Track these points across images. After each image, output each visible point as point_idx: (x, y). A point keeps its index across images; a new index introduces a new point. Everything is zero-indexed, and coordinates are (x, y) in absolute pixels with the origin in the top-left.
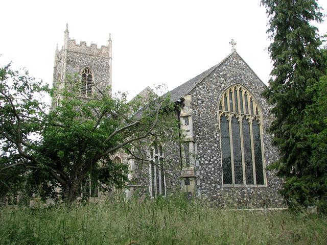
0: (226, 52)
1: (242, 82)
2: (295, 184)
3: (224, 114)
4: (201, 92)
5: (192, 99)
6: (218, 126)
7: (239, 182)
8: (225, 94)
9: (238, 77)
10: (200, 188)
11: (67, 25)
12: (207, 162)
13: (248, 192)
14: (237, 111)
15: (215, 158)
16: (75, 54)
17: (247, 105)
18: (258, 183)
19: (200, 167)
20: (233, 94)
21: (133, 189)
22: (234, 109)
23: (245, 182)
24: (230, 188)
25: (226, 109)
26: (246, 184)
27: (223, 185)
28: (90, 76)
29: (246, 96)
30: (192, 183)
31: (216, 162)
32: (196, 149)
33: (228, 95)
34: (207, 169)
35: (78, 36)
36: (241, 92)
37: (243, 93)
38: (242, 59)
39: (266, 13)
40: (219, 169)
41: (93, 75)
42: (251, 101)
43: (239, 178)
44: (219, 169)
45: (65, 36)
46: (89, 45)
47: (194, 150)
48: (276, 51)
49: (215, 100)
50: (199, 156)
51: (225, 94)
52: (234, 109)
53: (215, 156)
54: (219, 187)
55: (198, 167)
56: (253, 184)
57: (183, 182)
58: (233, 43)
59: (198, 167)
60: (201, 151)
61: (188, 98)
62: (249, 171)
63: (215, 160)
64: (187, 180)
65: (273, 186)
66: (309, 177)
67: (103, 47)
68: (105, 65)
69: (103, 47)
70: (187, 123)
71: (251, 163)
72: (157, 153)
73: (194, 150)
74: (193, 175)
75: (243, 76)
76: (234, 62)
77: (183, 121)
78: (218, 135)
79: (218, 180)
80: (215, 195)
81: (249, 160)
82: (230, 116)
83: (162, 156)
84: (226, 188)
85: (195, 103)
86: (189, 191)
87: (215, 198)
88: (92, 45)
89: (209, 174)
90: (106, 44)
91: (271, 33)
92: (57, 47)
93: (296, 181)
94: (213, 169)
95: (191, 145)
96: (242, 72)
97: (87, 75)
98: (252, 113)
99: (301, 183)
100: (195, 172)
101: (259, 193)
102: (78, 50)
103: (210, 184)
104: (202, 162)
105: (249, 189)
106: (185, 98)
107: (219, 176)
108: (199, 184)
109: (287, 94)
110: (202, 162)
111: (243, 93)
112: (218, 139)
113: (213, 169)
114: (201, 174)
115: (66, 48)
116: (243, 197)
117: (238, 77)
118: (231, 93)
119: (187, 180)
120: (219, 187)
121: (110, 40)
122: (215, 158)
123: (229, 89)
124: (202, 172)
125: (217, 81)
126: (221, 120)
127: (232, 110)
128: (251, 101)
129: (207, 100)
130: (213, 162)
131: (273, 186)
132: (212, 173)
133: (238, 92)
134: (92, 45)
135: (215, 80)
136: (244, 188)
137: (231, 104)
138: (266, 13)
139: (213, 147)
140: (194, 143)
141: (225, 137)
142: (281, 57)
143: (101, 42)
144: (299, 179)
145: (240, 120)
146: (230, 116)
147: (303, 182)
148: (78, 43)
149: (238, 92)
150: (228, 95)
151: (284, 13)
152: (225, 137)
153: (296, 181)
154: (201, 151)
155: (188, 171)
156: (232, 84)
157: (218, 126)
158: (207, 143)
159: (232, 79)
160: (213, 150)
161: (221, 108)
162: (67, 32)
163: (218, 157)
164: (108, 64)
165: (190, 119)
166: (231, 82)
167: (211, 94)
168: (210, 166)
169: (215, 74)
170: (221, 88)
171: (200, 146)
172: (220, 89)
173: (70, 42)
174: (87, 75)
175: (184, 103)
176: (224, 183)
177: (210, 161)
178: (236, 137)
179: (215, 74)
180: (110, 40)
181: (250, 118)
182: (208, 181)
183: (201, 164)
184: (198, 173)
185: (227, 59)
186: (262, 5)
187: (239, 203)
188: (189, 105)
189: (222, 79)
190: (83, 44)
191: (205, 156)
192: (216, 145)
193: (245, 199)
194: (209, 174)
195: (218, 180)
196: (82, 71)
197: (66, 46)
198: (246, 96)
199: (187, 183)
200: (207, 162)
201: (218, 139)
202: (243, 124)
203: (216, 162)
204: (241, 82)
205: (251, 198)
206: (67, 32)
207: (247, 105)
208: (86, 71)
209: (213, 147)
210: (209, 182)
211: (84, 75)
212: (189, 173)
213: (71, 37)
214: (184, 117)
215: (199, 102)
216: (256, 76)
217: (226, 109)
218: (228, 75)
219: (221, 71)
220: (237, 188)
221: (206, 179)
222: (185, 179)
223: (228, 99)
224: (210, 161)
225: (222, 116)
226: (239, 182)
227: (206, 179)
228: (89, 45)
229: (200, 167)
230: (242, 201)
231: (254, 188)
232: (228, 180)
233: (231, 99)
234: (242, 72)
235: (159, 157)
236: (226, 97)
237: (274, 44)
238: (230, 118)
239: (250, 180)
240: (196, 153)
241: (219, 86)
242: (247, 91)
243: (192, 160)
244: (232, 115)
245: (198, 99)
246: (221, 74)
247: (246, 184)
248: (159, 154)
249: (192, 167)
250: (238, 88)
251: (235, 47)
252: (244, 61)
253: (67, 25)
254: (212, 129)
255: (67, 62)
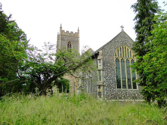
0: (119, 31)
1: (126, 44)
2: (145, 90)
3: (117, 58)
4: (107, 49)
5: (103, 52)
6: (114, 63)
7: (124, 88)
8: (118, 50)
9: (124, 42)
10: (106, 90)
11: (78, 28)
12: (109, 79)
13: (129, 92)
14: (124, 56)
15: (113, 77)
16: (64, 36)
17: (128, 54)
18: (134, 88)
19: (106, 81)
20: (122, 49)
21: (81, 90)
22: (127, 56)
24: (120, 90)
25: (118, 56)
26: (128, 88)
27: (117, 89)
28: (71, 45)
29: (128, 50)
30: (102, 88)
31: (113, 79)
32: (104, 73)
33: (119, 50)
34: (109, 82)
35: (65, 29)
36: (125, 48)
37: (127, 49)
38: (126, 34)
39: (134, 11)
40: (115, 82)
41: (72, 44)
42: (130, 52)
43: (124, 86)
44: (115, 82)
45: (60, 29)
46: (70, 32)
47: (103, 74)
48: (137, 28)
49: (113, 52)
50: (105, 76)
51: (118, 50)
52: (127, 56)
53: (113, 76)
54: (115, 90)
55: (105, 81)
56: (131, 89)
57: (98, 88)
58: (122, 27)
59: (105, 81)
60: (106, 74)
61: (101, 52)
62: (129, 83)
63: (113, 78)
64: (99, 86)
66: (153, 86)
67: (75, 33)
68: (77, 40)
69: (75, 33)
70: (100, 62)
71: (130, 79)
72: (90, 75)
73: (103, 74)
74: (102, 85)
75: (127, 41)
76: (122, 35)
77: (98, 61)
78: (114, 67)
79: (114, 87)
80: (113, 93)
81: (129, 78)
82: (120, 59)
83: (91, 76)
84: (118, 90)
85: (104, 54)
86: (100, 91)
87: (113, 95)
88: (71, 32)
89: (110, 84)
90: (77, 32)
91: (136, 21)
92: (58, 34)
93: (146, 88)
94: (112, 82)
95: (102, 71)
96: (126, 39)
97: (69, 44)
98: (131, 57)
99: (149, 89)
100: (103, 83)
101: (134, 93)
102: (66, 34)
103: (111, 88)
104: (107, 79)
105: (129, 91)
106: (99, 52)
107: (115, 85)
108: (105, 88)
109: (142, 48)
110: (107, 79)
111: (127, 49)
112: (114, 69)
114: (106, 84)
115: (61, 34)
116: (126, 94)
117: (124, 42)
118: (121, 49)
119: (99, 86)
120: (115, 90)
121: (78, 30)
122: (113, 77)
123: (120, 47)
124: (107, 83)
125: (114, 44)
126: (116, 60)
127: (121, 56)
128: (130, 52)
129: (109, 52)
130: (112, 79)
132: (111, 83)
133: (124, 48)
134: (71, 32)
135: (113, 44)
136: (127, 90)
137: (121, 54)
138: (134, 11)
139: (112, 72)
140: (103, 70)
141: (117, 68)
142: (139, 31)
143: (75, 31)
144: (148, 87)
145: (125, 60)
146: (120, 59)
147: (150, 89)
148: (65, 31)
149: (124, 48)
150: (119, 50)
151: (142, 10)
152: (117, 68)
153: (146, 88)
154: (106, 74)
155: (100, 83)
156: (121, 45)
157: (114, 63)
158: (109, 71)
159: (121, 43)
161: (116, 55)
162: (61, 27)
163: (114, 76)
164: (78, 40)
165: (101, 60)
166: (121, 44)
167: (111, 50)
168: (110, 81)
169: (113, 41)
170: (116, 47)
171: (106, 72)
172: (116, 47)
173: (62, 31)
174: (69, 44)
175: (99, 54)
176: (117, 88)
177: (111, 78)
178: (123, 68)
179: (113, 41)
180: (78, 30)
181: (125, 59)
182: (110, 87)
184: (105, 84)
185: (119, 34)
186: (132, 8)
187: (124, 97)
188: (101, 54)
189: (116, 43)
190: (68, 32)
191: (108, 76)
192: (113, 71)
193: (127, 95)
194: (110, 84)
195: (114, 87)
196: (67, 43)
197: (61, 33)
198: (128, 50)
199: (99, 88)
200: (109, 79)
201: (114, 69)
202: (121, 62)
203: (113, 79)
204: (126, 44)
205: (130, 95)
206: (61, 27)
207: (128, 54)
208: (69, 43)
209: (112, 72)
210: (110, 88)
211: (68, 45)
212: (101, 84)
213: (63, 29)
214: (99, 60)
215: (106, 53)
217: (118, 56)
218: (120, 41)
219: (116, 40)
220: (123, 90)
221: (109, 86)
222: (99, 86)
223: (119, 51)
224: (111, 78)
225: (116, 59)
226: (124, 88)
227: (109, 86)
228: (70, 32)
230: (126, 96)
231: (132, 91)
232: (119, 87)
233: (121, 51)
234: (126, 39)
235: (90, 76)
236: (118, 51)
237: (137, 25)
238: (120, 60)
239: (130, 87)
240: (104, 75)
241: (115, 46)
242: (126, 46)
243: (102, 78)
244: (121, 58)
245: (105, 52)
246: (116, 41)
247: (134, 88)
248: (90, 75)
249: (102, 81)
250: (124, 47)
251: (123, 29)
252: (127, 35)
254: (112, 64)
255: (61, 40)
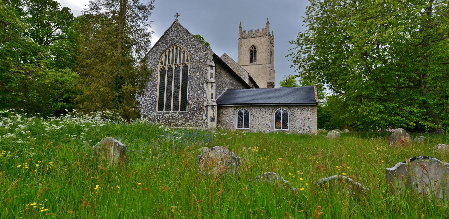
11: (268, 19)
19: (144, 102)
23: (172, 109)
65: (192, 111)
67: (263, 29)
82: (174, 68)
97: (253, 50)
113: (151, 102)
121: (268, 23)
130: (152, 98)
131: (192, 111)
160: (153, 91)
162: (240, 27)
174: (253, 50)
183: (145, 100)
206: (240, 27)
213: (243, 30)
216: (189, 33)
229: (144, 102)
239: (176, 108)
253: (268, 19)
